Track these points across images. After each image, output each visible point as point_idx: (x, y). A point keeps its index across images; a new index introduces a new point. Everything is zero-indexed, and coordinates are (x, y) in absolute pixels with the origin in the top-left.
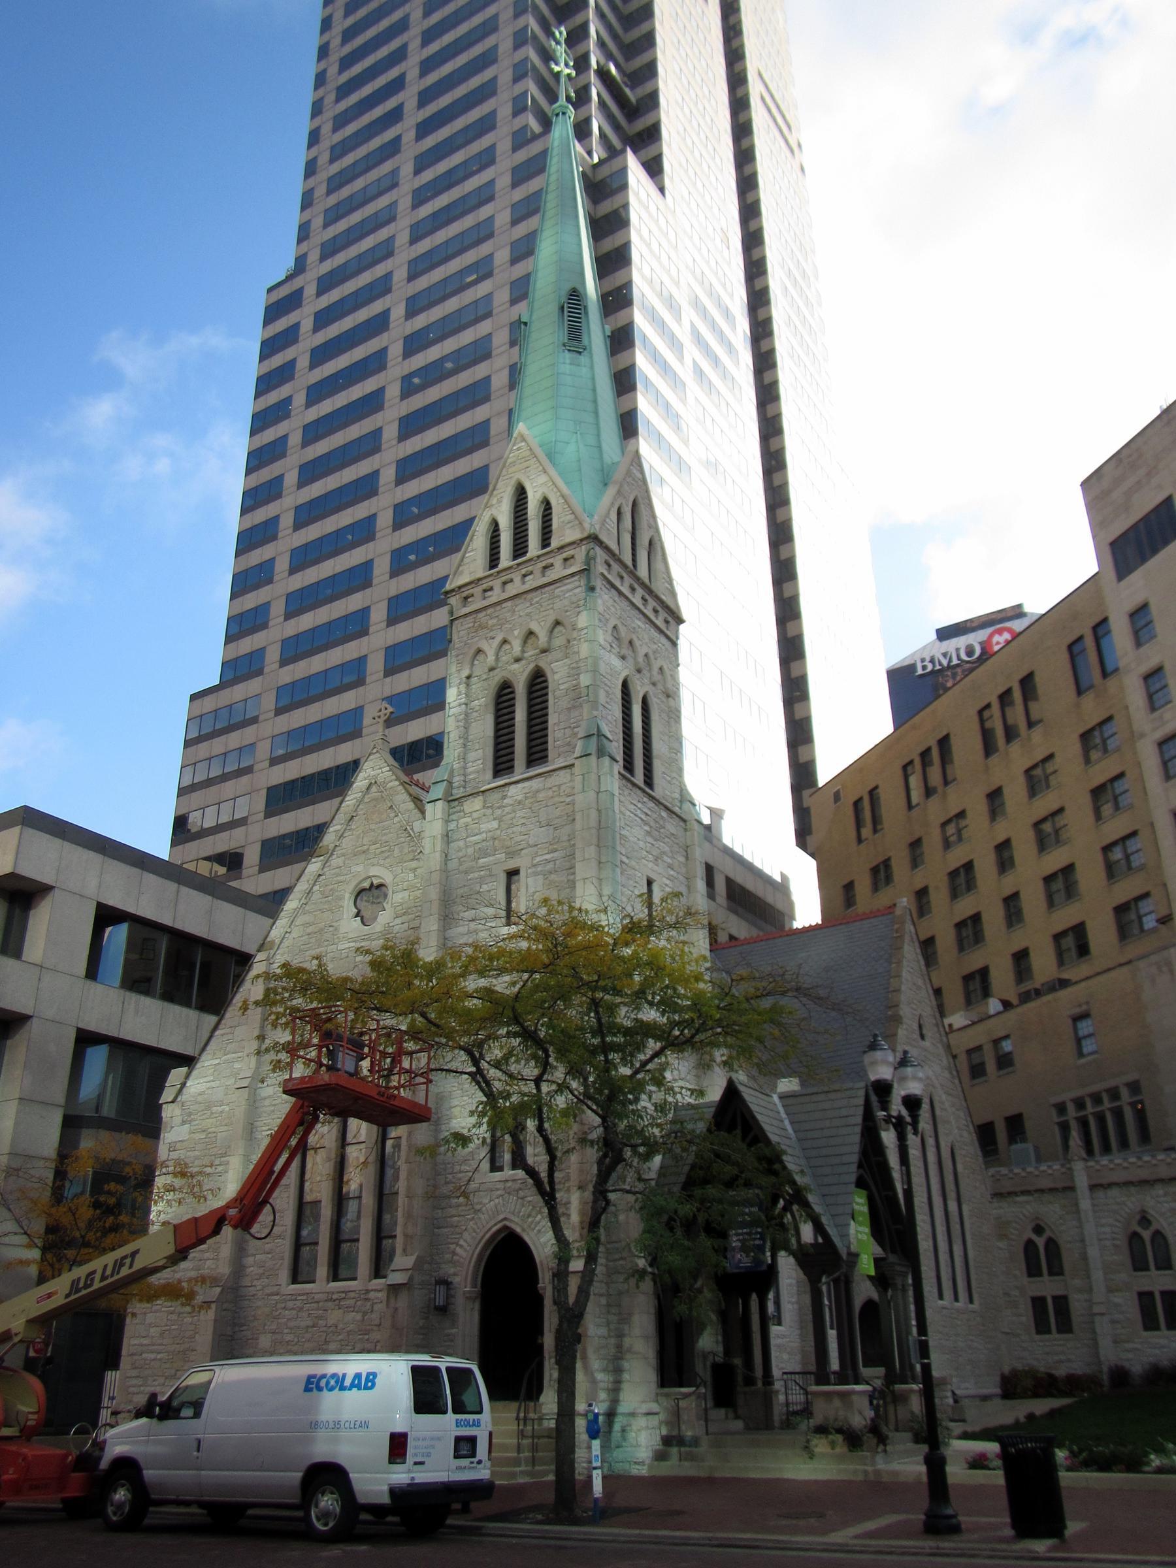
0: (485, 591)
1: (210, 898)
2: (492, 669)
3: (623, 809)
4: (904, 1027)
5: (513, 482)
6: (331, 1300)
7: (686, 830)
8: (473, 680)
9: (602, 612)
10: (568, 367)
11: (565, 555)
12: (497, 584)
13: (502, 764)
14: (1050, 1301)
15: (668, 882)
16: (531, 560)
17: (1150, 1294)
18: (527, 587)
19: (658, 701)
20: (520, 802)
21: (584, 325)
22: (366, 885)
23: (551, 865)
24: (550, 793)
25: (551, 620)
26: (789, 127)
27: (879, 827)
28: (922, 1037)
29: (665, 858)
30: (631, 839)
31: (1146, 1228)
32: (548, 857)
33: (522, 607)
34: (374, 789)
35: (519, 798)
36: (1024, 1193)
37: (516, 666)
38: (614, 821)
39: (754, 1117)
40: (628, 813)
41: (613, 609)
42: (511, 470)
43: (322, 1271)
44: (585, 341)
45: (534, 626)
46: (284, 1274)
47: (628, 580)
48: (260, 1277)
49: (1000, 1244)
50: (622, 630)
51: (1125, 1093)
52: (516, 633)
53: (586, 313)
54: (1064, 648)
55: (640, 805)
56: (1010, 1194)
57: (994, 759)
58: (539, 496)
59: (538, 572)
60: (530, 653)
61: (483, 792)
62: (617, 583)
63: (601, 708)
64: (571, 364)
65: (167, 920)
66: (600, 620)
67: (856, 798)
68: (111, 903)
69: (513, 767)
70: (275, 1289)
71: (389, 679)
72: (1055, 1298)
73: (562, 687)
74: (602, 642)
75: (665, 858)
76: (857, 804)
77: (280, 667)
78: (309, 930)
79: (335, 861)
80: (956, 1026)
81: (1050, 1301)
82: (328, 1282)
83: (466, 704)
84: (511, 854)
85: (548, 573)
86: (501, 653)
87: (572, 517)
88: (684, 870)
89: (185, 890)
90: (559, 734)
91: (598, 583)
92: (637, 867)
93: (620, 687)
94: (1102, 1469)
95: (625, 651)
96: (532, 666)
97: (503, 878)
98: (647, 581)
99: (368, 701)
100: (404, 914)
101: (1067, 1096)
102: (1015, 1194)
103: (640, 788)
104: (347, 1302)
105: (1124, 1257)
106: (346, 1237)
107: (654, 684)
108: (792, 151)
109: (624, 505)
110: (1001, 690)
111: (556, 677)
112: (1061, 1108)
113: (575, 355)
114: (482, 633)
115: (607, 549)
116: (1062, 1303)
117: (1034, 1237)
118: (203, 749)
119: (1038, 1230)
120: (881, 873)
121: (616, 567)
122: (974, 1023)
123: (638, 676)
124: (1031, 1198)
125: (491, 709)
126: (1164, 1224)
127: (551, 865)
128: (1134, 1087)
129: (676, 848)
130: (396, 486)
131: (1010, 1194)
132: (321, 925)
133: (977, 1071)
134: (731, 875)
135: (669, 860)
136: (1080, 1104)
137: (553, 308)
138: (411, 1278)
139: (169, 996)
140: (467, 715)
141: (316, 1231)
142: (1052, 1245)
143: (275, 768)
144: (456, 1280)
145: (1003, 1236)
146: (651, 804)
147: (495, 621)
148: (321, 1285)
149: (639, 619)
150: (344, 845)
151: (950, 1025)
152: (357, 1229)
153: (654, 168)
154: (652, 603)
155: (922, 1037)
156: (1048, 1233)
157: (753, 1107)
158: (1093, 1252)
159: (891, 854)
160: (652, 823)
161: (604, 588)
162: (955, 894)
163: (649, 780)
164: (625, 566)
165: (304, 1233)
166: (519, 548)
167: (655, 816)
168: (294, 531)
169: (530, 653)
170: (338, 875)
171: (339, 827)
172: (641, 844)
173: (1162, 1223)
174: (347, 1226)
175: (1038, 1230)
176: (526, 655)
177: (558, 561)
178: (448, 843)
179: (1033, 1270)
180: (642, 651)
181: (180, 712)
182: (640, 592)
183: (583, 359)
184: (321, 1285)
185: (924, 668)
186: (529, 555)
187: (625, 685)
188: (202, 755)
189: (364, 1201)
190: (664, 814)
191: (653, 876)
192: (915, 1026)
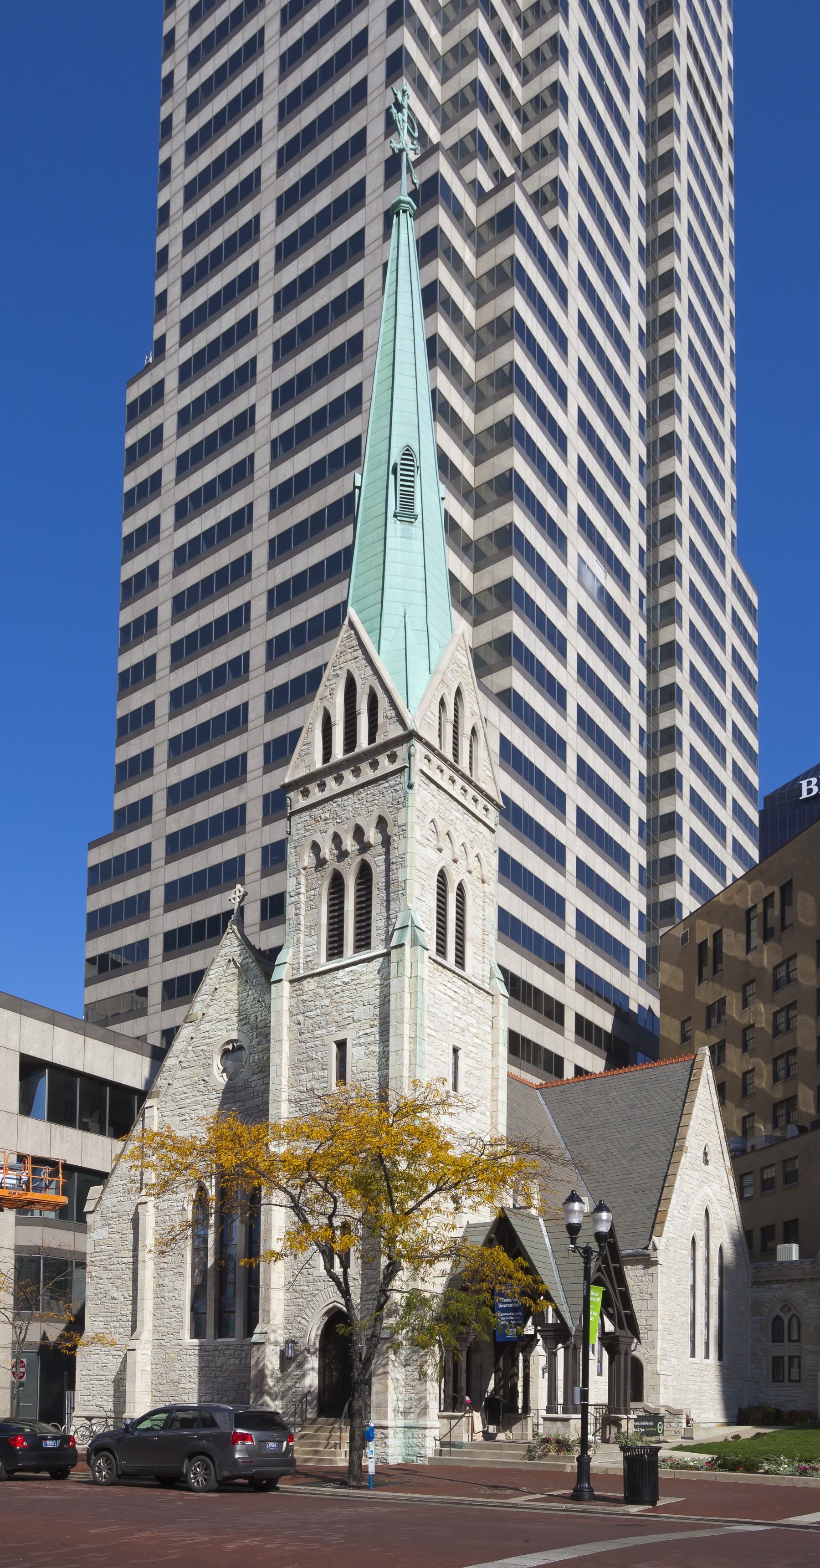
1: (112, 1047)
3: (433, 990)
4: (689, 1155)
7: (493, 1003)
9: (420, 808)
10: (399, 540)
13: (335, 948)
15: (473, 1049)
19: (473, 888)
27: (719, 967)
28: (706, 1162)
29: (471, 1029)
30: (440, 1015)
35: (346, 980)
36: (777, 1282)
38: (423, 1002)
39: (517, 1236)
40: (438, 993)
41: (431, 804)
44: (418, 510)
45: (360, 821)
47: (448, 772)
50: (439, 822)
55: (449, 985)
56: (767, 1282)
62: (437, 777)
63: (415, 900)
64: (402, 537)
66: (418, 817)
68: (31, 1053)
70: (177, 1342)
71: (267, 828)
74: (419, 838)
75: (471, 1029)
77: (167, 815)
78: (186, 1083)
80: (758, 1147)
82: (215, 1339)
84: (341, 1027)
91: (417, 779)
92: (444, 1038)
93: (436, 877)
94: (731, 1470)
95: (445, 844)
98: (468, 773)
99: (248, 849)
100: (260, 1072)
102: (772, 1282)
103: (450, 970)
104: (229, 1352)
107: (470, 872)
109: (447, 694)
115: (427, 745)
121: (436, 761)
123: (454, 865)
124: (783, 1286)
130: (267, 620)
131: (767, 1282)
133: (767, 1185)
135: (475, 1031)
139: (84, 1127)
146: (460, 983)
149: (457, 811)
151: (753, 1147)
154: (472, 792)
155: (706, 1162)
156: (793, 1311)
157: (516, 1228)
160: (461, 1000)
161: (422, 784)
163: (460, 961)
164: (444, 760)
167: (462, 993)
168: (171, 671)
170: (205, 1038)
172: (449, 1019)
175: (786, 1308)
182: (460, 782)
183: (416, 529)
187: (442, 875)
189: (237, 1285)
191: (458, 1045)
192: (701, 1154)
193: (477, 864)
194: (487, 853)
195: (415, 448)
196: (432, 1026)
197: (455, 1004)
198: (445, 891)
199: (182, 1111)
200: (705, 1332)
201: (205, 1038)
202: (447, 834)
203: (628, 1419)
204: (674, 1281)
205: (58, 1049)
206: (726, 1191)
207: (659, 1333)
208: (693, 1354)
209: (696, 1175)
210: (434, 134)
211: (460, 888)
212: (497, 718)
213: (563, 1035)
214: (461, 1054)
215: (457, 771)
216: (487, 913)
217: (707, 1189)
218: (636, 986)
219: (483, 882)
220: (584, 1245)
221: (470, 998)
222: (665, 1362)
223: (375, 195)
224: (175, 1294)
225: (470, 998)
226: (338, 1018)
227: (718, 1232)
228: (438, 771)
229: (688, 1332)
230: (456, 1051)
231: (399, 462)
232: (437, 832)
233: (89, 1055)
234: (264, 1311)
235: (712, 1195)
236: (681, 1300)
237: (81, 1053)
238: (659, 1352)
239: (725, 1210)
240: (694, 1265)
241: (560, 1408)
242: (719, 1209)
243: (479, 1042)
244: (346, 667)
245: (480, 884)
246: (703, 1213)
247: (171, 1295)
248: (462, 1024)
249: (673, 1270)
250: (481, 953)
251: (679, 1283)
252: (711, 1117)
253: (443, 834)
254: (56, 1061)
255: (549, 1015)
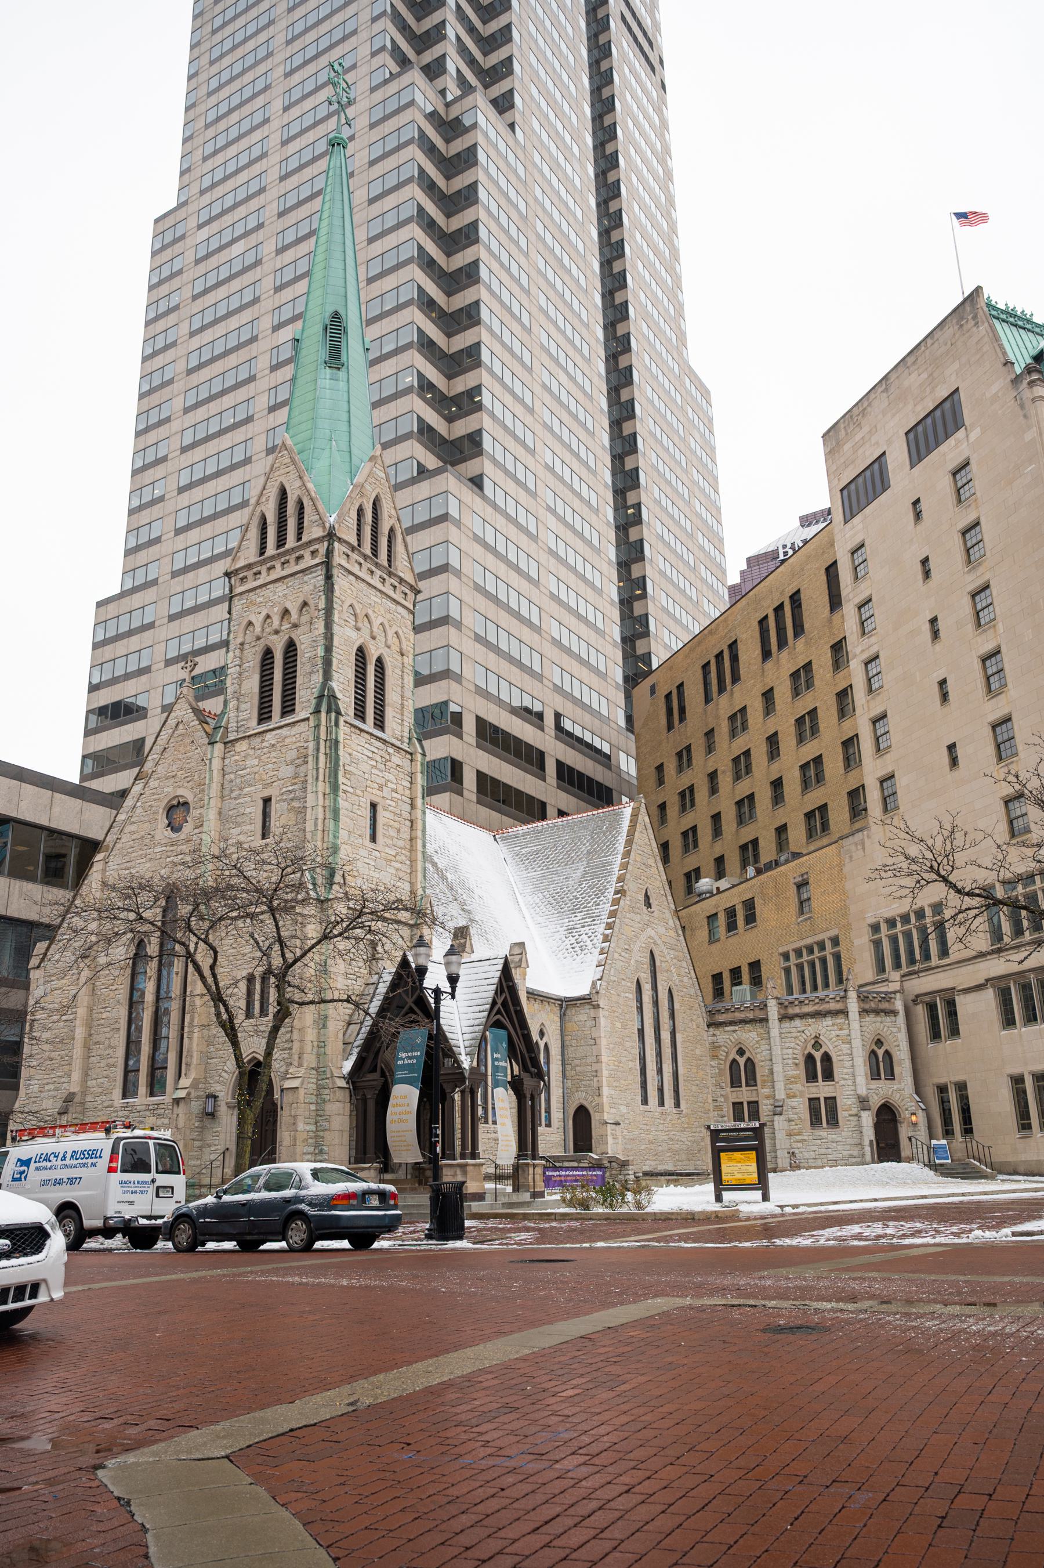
0: (255, 574)
2: (258, 638)
5: (277, 484)
6: (148, 1110)
7: (412, 761)
8: (246, 646)
11: (312, 549)
12: (263, 569)
13: (264, 715)
14: (745, 1105)
15: (391, 803)
16: (288, 551)
17: (742, 1103)
18: (285, 573)
20: (273, 745)
21: (343, 344)
22: (175, 802)
23: (292, 795)
24: (294, 739)
25: (300, 600)
26: (651, 44)
31: (817, 1051)
32: (290, 788)
33: (280, 587)
34: (181, 726)
35: (273, 742)
37: (275, 637)
42: (277, 473)
43: (142, 1089)
44: (344, 358)
45: (289, 606)
46: (117, 1093)
48: (101, 1094)
49: (713, 1063)
51: (828, 945)
52: (276, 610)
53: (346, 332)
54: (823, 571)
55: (367, 746)
57: (770, 664)
58: (295, 497)
59: (292, 561)
60: (286, 626)
61: (249, 736)
62: (355, 569)
65: (44, 822)
67: (666, 693)
69: (271, 717)
72: (749, 1103)
73: (307, 655)
75: (389, 784)
76: (668, 696)
78: (134, 837)
79: (153, 783)
81: (745, 1105)
83: (240, 666)
84: (267, 786)
85: (300, 561)
86: (266, 626)
87: (317, 517)
88: (408, 792)
89: (57, 796)
90: (302, 693)
95: (364, 625)
96: (287, 637)
97: (261, 803)
101: (789, 948)
105: (801, 1072)
106: (159, 1065)
107: (389, 647)
108: (653, 69)
110: (777, 604)
111: (303, 647)
112: (786, 956)
113: (335, 371)
114: (252, 608)
116: (831, 1101)
117: (738, 1058)
118: (108, 652)
119: (741, 1052)
120: (684, 756)
122: (734, 886)
123: (372, 642)
124: (737, 1028)
125: (258, 670)
126: (831, 1048)
127: (292, 795)
128: (835, 941)
129: (401, 775)
132: (143, 833)
134: (562, 759)
136: (799, 952)
137: (318, 328)
138: (189, 1094)
140: (240, 674)
141: (138, 1061)
142: (827, 1058)
143: (170, 668)
144: (221, 1095)
145: (714, 1057)
147: (261, 599)
148: (142, 1098)
150: (159, 771)
152: (166, 1060)
153: (503, 104)
156: (747, 1055)
158: (778, 1068)
159: (692, 741)
162: (737, 777)
163: (380, 724)
165: (131, 1063)
166: (281, 541)
169: (286, 626)
170: (154, 794)
171: (155, 756)
172: (367, 776)
173: (828, 1046)
174: (160, 1057)
175: (741, 1052)
176: (283, 628)
177: (307, 553)
178: (224, 776)
179: (735, 1083)
180: (376, 623)
181: (89, 616)
183: (342, 374)
184: (142, 1098)
185: (785, 553)
186: (287, 546)
188: (107, 657)
190: (391, 750)
191: (376, 799)
192: (642, 898)
193: (396, 640)
194: (405, 630)
195: (342, 312)
196: (348, 783)
197: (374, 763)
198: (365, 664)
199: (128, 865)
200: (657, 1078)
201: (154, 794)
202: (366, 616)
203: (534, 1166)
204: (618, 1025)
205: (23, 805)
206: (672, 933)
207: (604, 1079)
208: (645, 1101)
209: (637, 918)
210: (410, 53)
211: (380, 661)
212: (470, 499)
213: (544, 780)
214: (379, 809)
215: (377, 565)
216: (406, 681)
217: (650, 932)
218: (553, 740)
219: (402, 655)
220: (434, 987)
221: (388, 757)
222: (613, 1111)
223: (363, 96)
224: (110, 1051)
225: (388, 757)
226: (265, 777)
227: (666, 974)
228: (357, 566)
229: (638, 1079)
230: (374, 806)
231: (328, 323)
232: (355, 615)
233: (56, 809)
234: (187, 1064)
235: (656, 938)
236: (628, 1044)
237: (48, 808)
238: (605, 1100)
239: (672, 952)
240: (640, 1009)
241: (458, 1155)
242: (666, 952)
243: (399, 796)
244: (280, 479)
245: (399, 658)
246: (648, 955)
247: (107, 1052)
248: (382, 781)
249: (616, 1014)
250: (399, 716)
251: (624, 1027)
252: (651, 862)
253: (361, 617)
254: (20, 817)
255: (530, 761)
